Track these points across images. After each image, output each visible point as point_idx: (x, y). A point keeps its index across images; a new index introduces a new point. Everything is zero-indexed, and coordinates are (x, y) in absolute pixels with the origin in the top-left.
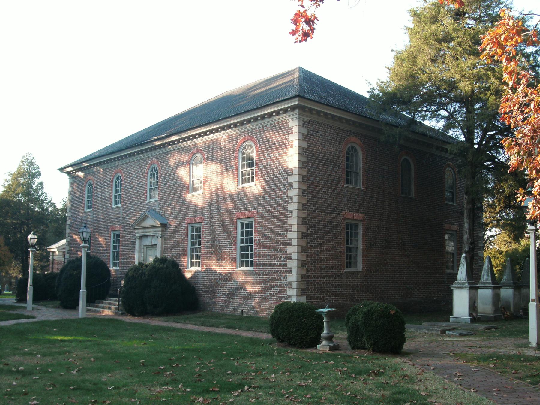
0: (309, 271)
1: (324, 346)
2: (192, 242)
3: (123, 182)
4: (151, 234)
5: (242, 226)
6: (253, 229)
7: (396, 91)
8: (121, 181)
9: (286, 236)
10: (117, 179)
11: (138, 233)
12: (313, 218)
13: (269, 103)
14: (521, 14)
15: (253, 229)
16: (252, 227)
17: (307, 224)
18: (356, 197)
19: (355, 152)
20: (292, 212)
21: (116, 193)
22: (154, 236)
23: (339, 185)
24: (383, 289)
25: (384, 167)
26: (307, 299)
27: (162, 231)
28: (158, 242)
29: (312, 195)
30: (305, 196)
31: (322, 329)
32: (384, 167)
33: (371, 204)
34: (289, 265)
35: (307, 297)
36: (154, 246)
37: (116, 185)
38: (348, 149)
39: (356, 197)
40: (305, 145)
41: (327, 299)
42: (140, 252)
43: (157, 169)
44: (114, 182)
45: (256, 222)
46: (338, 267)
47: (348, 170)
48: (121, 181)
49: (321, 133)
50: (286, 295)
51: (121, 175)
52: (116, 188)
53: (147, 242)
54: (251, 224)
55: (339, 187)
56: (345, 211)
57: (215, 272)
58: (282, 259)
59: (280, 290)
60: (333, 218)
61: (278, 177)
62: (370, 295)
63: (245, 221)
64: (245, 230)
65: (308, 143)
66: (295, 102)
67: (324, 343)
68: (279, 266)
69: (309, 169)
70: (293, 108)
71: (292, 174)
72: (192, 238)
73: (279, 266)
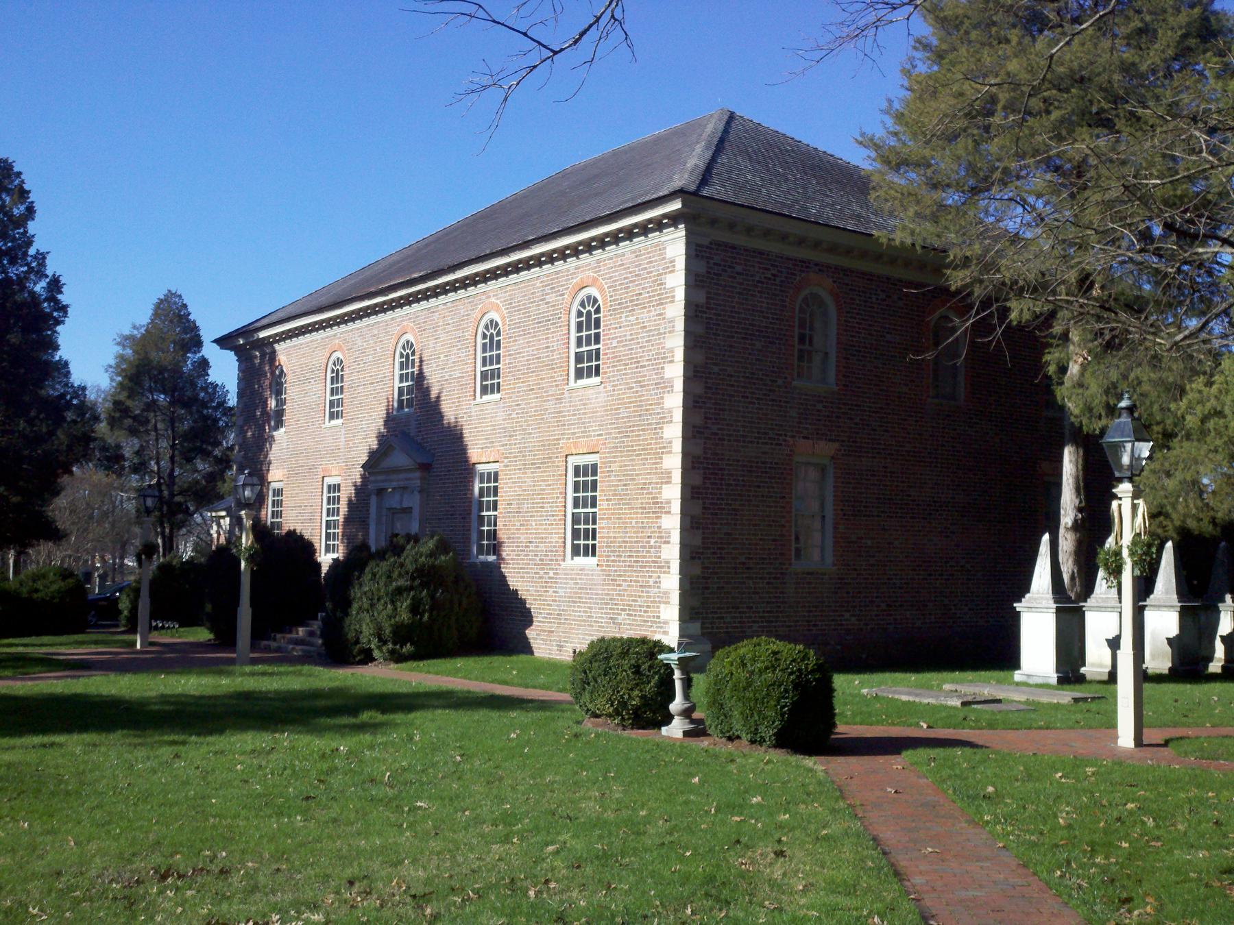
0: (708, 568)
1: (675, 729)
3: (346, 371)
4: (402, 484)
9: (660, 493)
10: (404, 348)
11: (376, 481)
12: (717, 454)
13: (648, 198)
14: (134, 327)
17: (705, 468)
18: (820, 407)
20: (670, 442)
22: (405, 488)
23: (780, 382)
24: (883, 606)
25: (888, 337)
26: (702, 628)
27: (422, 479)
28: (414, 501)
29: (715, 404)
30: (701, 407)
31: (672, 698)
32: (888, 337)
33: (857, 420)
34: (664, 556)
35: (703, 623)
36: (408, 511)
39: (820, 407)
40: (701, 298)
41: (750, 627)
42: (378, 523)
43: (497, 324)
44: (574, 314)
46: (776, 559)
49: (739, 268)
50: (658, 617)
53: (394, 502)
54: (594, 467)
55: (779, 387)
56: (793, 437)
58: (652, 542)
59: (648, 607)
60: (764, 453)
61: (644, 366)
62: (853, 619)
63: (582, 460)
65: (708, 293)
66: (676, 205)
67: (677, 721)
68: (644, 557)
69: (710, 348)
70: (673, 220)
71: (671, 362)
73: (644, 557)
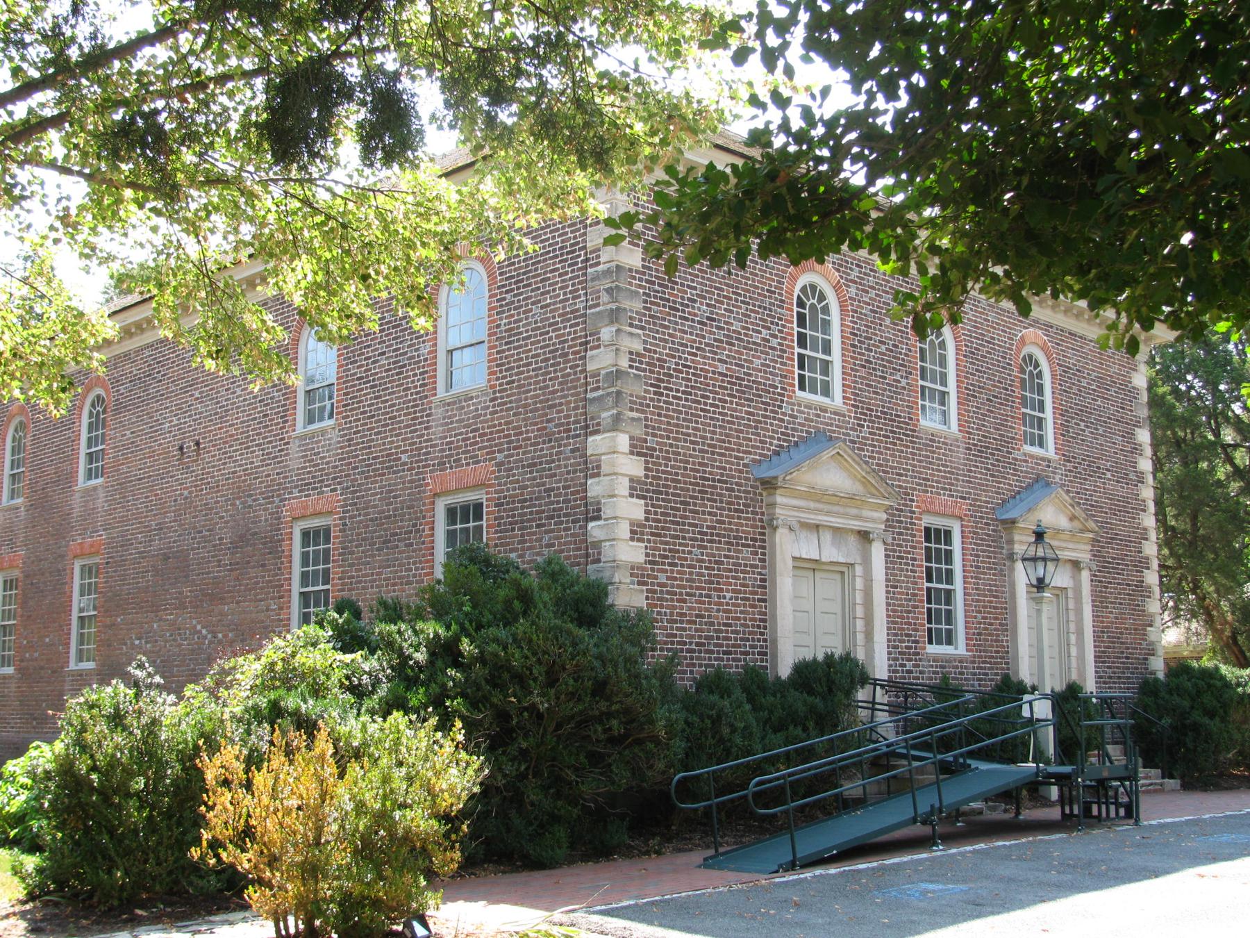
2: (304, 576)
5: (451, 513)
6: (484, 523)
7: (664, 717)
8: (104, 412)
15: (484, 523)
16: (479, 517)
19: (820, 301)
21: (89, 447)
37: (90, 424)
38: (804, 289)
45: (487, 500)
47: (802, 351)
48: (104, 412)
51: (103, 393)
52: (90, 432)
54: (478, 507)
57: (204, 780)
64: (311, 568)
72: (305, 562)
